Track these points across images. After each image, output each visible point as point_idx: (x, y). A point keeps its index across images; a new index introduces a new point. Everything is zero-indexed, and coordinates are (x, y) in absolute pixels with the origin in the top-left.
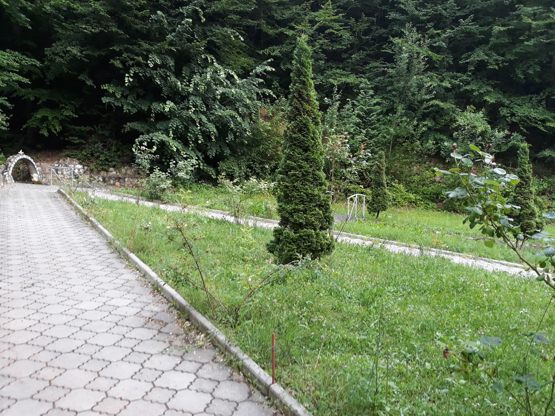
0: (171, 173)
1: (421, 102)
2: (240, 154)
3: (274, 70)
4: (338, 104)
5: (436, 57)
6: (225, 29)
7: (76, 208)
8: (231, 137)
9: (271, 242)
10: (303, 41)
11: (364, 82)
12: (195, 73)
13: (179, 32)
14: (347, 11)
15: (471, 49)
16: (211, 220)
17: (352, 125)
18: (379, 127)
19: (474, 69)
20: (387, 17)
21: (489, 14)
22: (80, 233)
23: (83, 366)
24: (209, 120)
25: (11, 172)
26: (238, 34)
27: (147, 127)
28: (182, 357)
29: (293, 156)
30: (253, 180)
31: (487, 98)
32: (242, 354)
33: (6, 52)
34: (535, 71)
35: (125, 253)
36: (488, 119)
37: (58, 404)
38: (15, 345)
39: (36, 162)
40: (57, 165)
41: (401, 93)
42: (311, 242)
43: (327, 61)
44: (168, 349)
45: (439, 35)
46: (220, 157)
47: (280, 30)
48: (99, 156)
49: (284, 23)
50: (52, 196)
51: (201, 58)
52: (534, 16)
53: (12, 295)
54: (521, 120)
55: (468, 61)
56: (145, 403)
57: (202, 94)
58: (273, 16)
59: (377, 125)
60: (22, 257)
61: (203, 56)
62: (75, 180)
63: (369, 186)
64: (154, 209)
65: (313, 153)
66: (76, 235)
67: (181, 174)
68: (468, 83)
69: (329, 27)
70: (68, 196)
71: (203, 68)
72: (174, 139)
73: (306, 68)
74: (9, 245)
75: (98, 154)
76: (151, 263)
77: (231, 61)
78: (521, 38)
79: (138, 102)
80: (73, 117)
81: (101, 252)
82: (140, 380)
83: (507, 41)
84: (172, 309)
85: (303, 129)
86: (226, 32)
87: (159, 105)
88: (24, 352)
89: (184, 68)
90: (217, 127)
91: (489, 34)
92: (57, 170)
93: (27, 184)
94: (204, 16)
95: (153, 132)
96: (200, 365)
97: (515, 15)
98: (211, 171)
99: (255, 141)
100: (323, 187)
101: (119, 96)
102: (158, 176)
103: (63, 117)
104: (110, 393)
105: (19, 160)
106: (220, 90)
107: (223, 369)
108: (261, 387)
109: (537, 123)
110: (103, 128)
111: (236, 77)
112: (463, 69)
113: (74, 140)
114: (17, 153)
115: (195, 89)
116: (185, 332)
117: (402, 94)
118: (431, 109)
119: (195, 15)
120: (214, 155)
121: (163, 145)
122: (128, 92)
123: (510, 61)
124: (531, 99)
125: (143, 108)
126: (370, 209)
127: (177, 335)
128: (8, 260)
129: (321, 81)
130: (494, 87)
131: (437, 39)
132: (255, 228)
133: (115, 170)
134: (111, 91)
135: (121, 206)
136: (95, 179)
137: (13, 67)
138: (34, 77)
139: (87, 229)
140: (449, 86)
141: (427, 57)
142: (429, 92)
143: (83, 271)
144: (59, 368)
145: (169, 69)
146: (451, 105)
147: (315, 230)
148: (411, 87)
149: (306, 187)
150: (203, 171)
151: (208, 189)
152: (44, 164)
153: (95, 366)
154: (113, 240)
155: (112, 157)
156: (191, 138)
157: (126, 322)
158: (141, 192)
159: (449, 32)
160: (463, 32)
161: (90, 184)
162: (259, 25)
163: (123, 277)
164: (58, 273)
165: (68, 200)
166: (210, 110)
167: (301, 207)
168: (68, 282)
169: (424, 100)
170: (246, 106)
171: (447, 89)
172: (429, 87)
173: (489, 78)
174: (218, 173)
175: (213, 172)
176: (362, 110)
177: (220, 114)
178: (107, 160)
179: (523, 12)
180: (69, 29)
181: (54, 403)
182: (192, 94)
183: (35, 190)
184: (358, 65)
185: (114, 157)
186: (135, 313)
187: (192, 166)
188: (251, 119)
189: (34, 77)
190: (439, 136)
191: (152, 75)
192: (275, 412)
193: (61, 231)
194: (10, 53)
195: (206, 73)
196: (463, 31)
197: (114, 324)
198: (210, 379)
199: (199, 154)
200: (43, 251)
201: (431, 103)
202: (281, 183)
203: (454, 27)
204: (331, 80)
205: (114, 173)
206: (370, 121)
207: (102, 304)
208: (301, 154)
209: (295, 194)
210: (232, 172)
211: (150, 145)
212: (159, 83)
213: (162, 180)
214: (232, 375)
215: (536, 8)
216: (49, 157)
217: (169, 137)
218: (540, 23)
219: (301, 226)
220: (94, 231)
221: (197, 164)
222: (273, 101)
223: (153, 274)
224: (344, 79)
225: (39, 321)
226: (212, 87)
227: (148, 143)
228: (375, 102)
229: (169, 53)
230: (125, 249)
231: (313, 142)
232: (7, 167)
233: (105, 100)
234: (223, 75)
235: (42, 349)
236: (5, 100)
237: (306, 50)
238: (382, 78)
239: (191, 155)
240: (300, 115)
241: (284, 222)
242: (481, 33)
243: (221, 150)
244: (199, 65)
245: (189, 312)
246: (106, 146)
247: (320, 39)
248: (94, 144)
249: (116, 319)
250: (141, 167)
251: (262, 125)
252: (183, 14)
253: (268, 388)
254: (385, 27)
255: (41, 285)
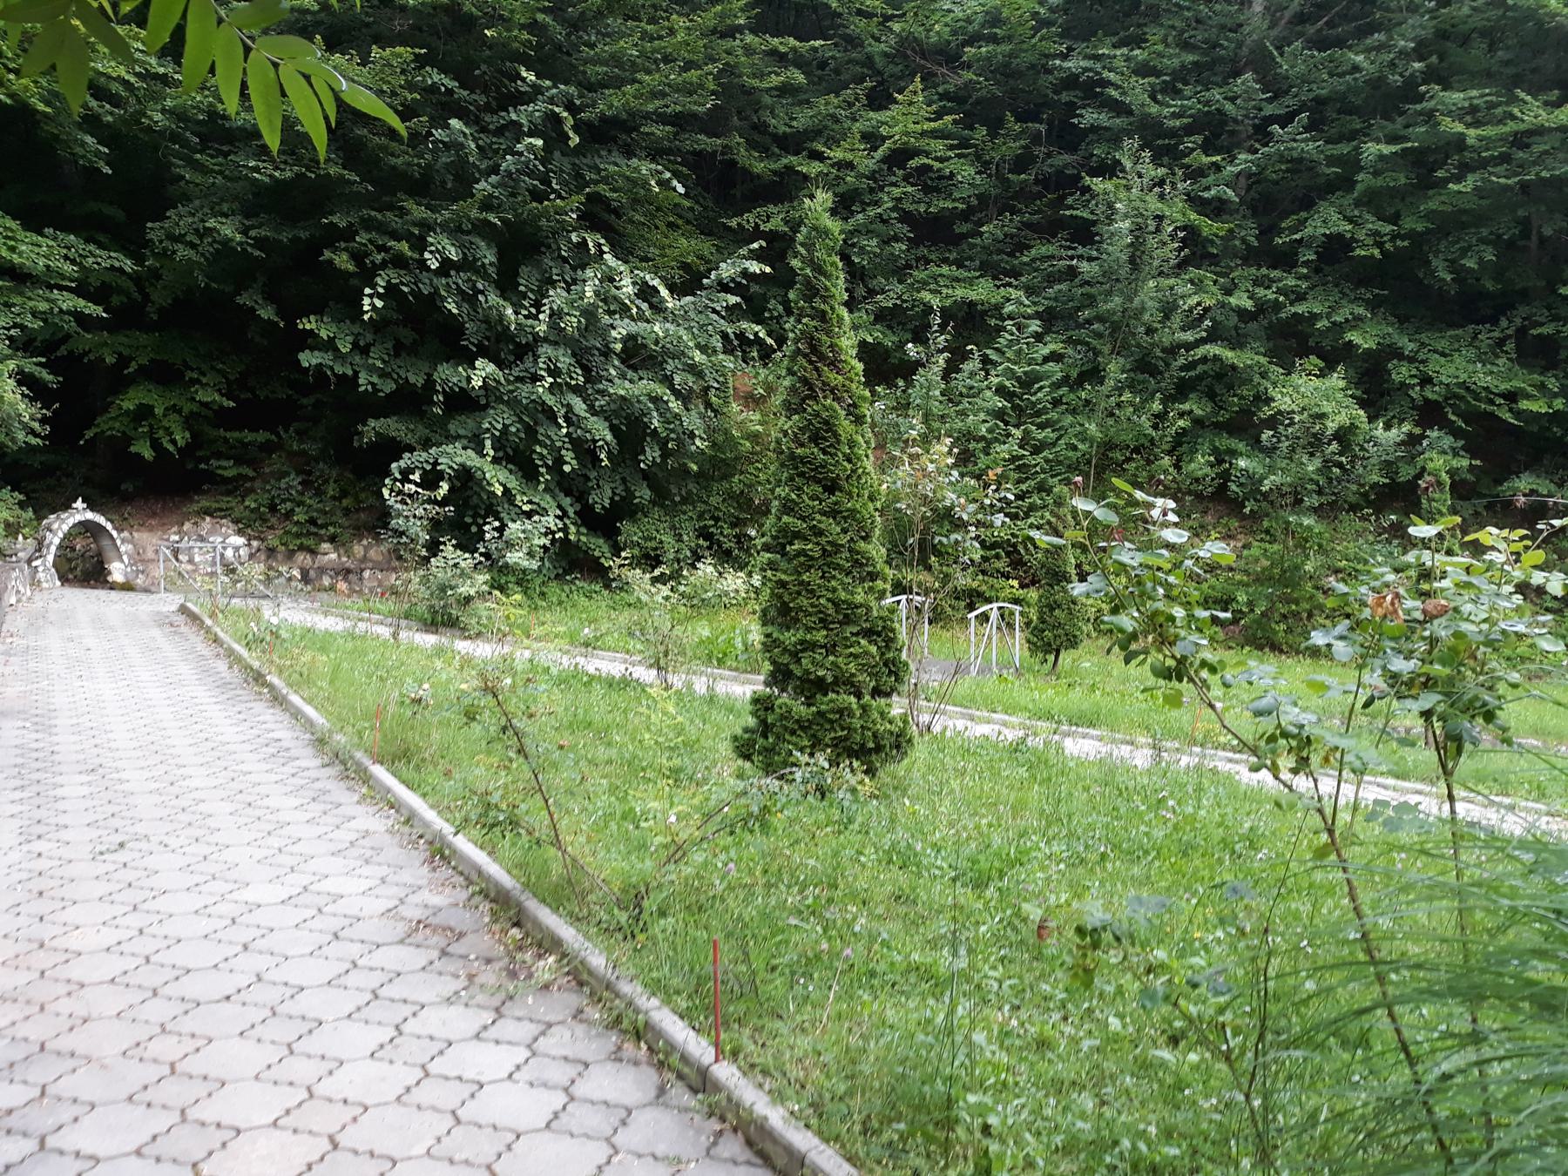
0: (487, 555)
1: (1173, 350)
2: (677, 499)
3: (768, 270)
4: (941, 360)
5: (1209, 227)
6: (634, 162)
7: (230, 653)
8: (652, 454)
9: (746, 730)
10: (819, 209)
11: (1015, 299)
12: (553, 283)
13: (509, 174)
14: (968, 107)
15: (1307, 203)
16: (592, 678)
17: (982, 416)
18: (1059, 421)
19: (1313, 257)
20: (1075, 121)
21: (1350, 110)
22: (241, 717)
23: (252, 1032)
24: (592, 409)
25: (50, 558)
26: (668, 175)
27: (422, 431)
28: (497, 1010)
29: (797, 504)
30: (706, 569)
31: (1354, 337)
32: (644, 998)
33: (43, 235)
34: (1481, 261)
35: (358, 764)
36: (1358, 393)
37: (193, 1114)
38: (83, 986)
39: (120, 530)
40: (177, 538)
41: (1115, 327)
42: (849, 729)
43: (914, 243)
44: (463, 993)
45: (1217, 167)
46: (624, 509)
47: (785, 161)
48: (292, 510)
49: (795, 143)
50: (163, 622)
51: (570, 241)
52: (1473, 115)
53: (69, 871)
54: (1450, 396)
55: (1297, 236)
56: (402, 1110)
57: (572, 337)
58: (766, 125)
59: (1053, 415)
60: (89, 778)
61: (574, 238)
62: (226, 579)
63: (1033, 583)
64: (439, 651)
65: (850, 494)
66: (229, 721)
67: (515, 557)
68: (1301, 298)
69: (917, 152)
70: (209, 622)
71: (574, 269)
72: (495, 461)
73: (828, 276)
74: (56, 748)
75: (289, 505)
76: (428, 788)
77: (652, 249)
78: (1440, 174)
79: (398, 362)
80: (221, 407)
81: (297, 763)
82: (391, 1062)
83: (1403, 181)
84: (477, 899)
85: (821, 433)
86: (637, 170)
87: (456, 371)
88: (107, 1002)
89: (524, 270)
90: (613, 429)
91: (1352, 164)
92: (176, 552)
93: (96, 592)
94: (576, 128)
95: (439, 445)
96: (542, 1027)
97: (1421, 113)
98: (598, 546)
99: (720, 465)
100: (879, 582)
101: (345, 348)
102: (451, 563)
103: (195, 408)
104: (319, 1089)
105: (75, 525)
106: (622, 329)
107: (598, 1035)
108: (686, 1070)
109: (1492, 402)
110: (302, 435)
111: (664, 292)
112: (1285, 259)
113: (225, 468)
114: (70, 507)
115: (554, 326)
116: (509, 953)
117: (1118, 330)
118: (1200, 369)
119: (550, 128)
120: (607, 503)
121: (465, 478)
122: (369, 337)
123: (1411, 235)
124: (1475, 337)
125: (412, 379)
126: (1034, 644)
127: (488, 961)
128: (55, 786)
129: (899, 298)
130: (1373, 305)
131: (1211, 178)
132: (711, 699)
133: (336, 549)
134: (324, 334)
135: (350, 645)
136: (281, 574)
137: (63, 277)
138: (116, 300)
139: (259, 707)
140: (1248, 304)
141: (1184, 228)
142: (1192, 323)
143: (249, 811)
144: (193, 1036)
145: (481, 271)
146: (1257, 358)
147: (859, 696)
148: (1143, 309)
149: (833, 583)
150: (576, 546)
151: (590, 598)
152: (141, 536)
153: (283, 1031)
154: (330, 732)
155: (326, 513)
156: (542, 457)
157: (360, 930)
158: (406, 606)
159: (1244, 160)
160: (1282, 158)
161: (267, 587)
162: (727, 149)
163: (353, 824)
164: (185, 818)
165: (208, 630)
166: (594, 383)
167: (820, 636)
168: (213, 839)
169: (1179, 346)
170: (694, 370)
171: (1241, 313)
172: (1191, 310)
173: (1360, 283)
174: (616, 551)
175: (606, 549)
176: (1010, 374)
177: (622, 392)
178: (312, 521)
179: (1443, 103)
180: (213, 171)
181: (183, 1112)
182: (546, 340)
183: (117, 606)
184: (1000, 252)
185: (332, 513)
186: (383, 910)
187: (546, 534)
188: (708, 405)
189: (116, 300)
190: (1225, 442)
191: (437, 290)
192: (718, 1127)
193: (190, 711)
194: (55, 239)
195: (584, 281)
196: (1282, 156)
197: (330, 937)
198: (566, 1058)
199: (566, 502)
200: (143, 763)
201: (1201, 351)
202: (769, 573)
203: (1257, 146)
204: (926, 296)
205: (333, 556)
206: (1034, 404)
207: (300, 890)
208: (818, 499)
209: (804, 602)
210: (656, 549)
211: (431, 479)
212: (455, 311)
213: (463, 574)
214: (619, 1048)
215: (1474, 93)
216: (154, 515)
217: (484, 456)
218: (1489, 131)
219: (821, 686)
220: (277, 711)
221: (560, 530)
222: (766, 355)
223: (430, 815)
224: (960, 292)
225: (141, 932)
226: (599, 320)
227: (425, 474)
228: (1045, 351)
229: (483, 228)
230: (359, 755)
231: (849, 466)
232: (40, 545)
233: (308, 359)
234: (627, 288)
235: (150, 994)
236: (37, 364)
237: (826, 233)
238: (1063, 287)
239: (543, 504)
240: (815, 398)
241: (780, 676)
242: (1332, 161)
243: (627, 490)
244: (565, 260)
245: (519, 905)
246: (312, 482)
247: (894, 184)
248: (279, 480)
249: (336, 924)
250: (404, 539)
251: (739, 419)
252: (521, 125)
253: (704, 1073)
254: (1072, 148)
255: (144, 845)
